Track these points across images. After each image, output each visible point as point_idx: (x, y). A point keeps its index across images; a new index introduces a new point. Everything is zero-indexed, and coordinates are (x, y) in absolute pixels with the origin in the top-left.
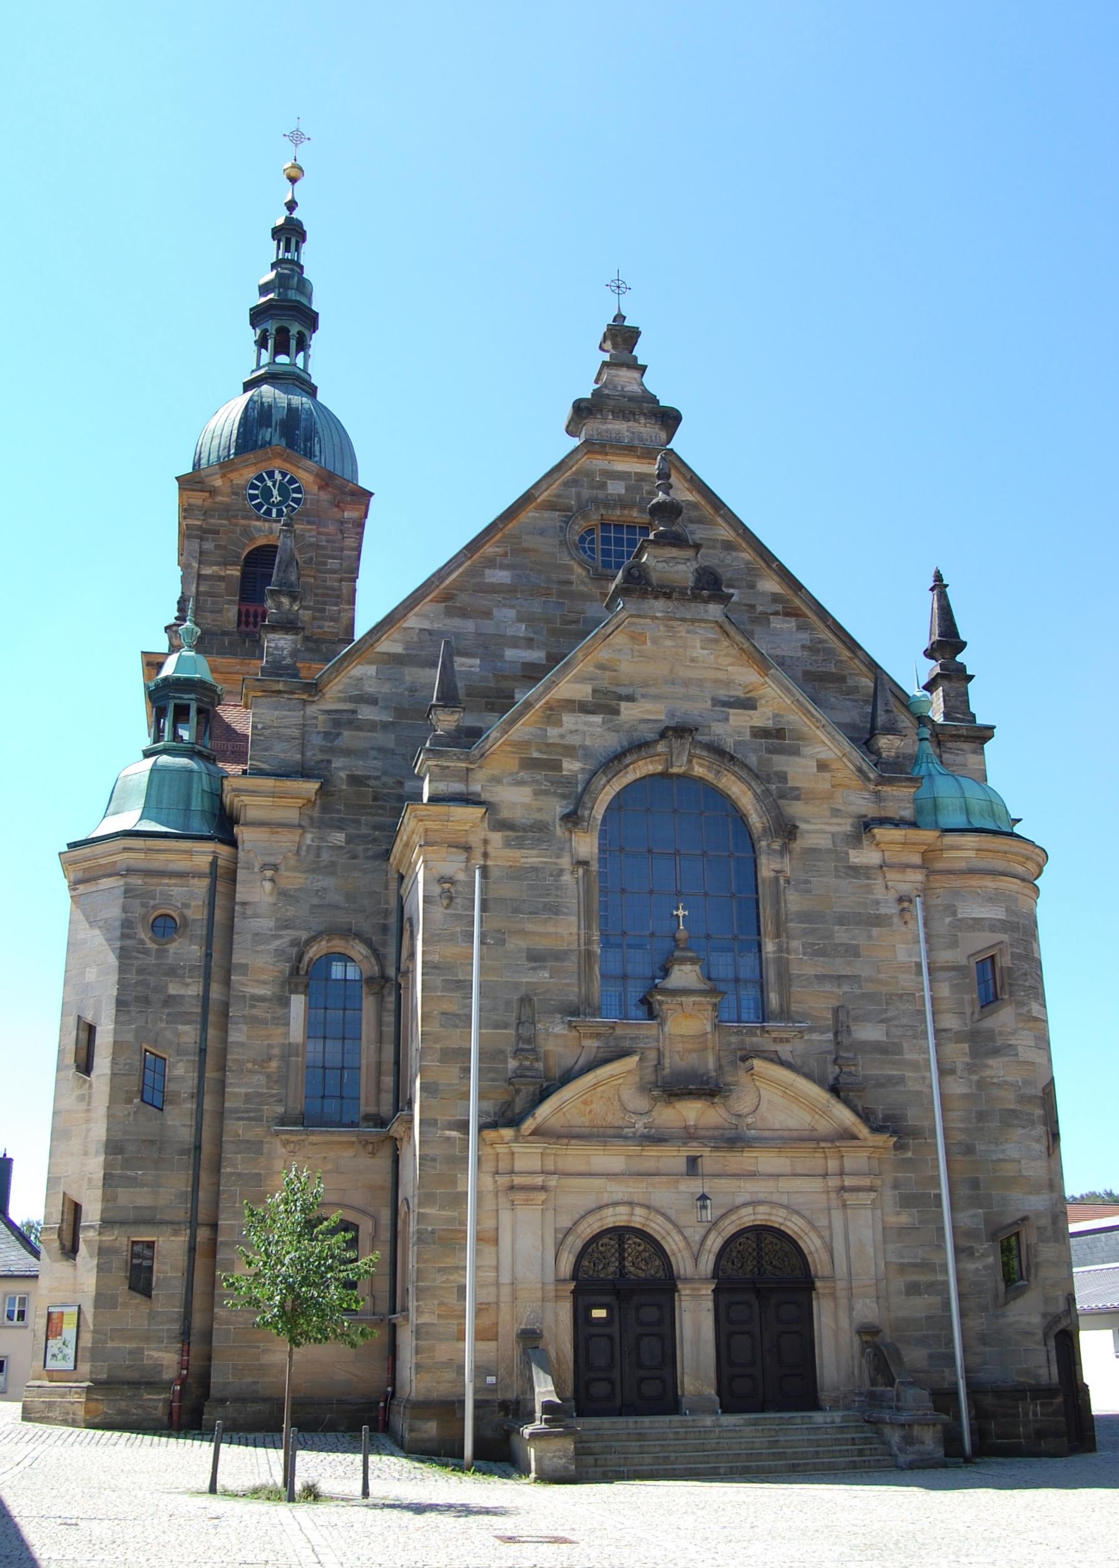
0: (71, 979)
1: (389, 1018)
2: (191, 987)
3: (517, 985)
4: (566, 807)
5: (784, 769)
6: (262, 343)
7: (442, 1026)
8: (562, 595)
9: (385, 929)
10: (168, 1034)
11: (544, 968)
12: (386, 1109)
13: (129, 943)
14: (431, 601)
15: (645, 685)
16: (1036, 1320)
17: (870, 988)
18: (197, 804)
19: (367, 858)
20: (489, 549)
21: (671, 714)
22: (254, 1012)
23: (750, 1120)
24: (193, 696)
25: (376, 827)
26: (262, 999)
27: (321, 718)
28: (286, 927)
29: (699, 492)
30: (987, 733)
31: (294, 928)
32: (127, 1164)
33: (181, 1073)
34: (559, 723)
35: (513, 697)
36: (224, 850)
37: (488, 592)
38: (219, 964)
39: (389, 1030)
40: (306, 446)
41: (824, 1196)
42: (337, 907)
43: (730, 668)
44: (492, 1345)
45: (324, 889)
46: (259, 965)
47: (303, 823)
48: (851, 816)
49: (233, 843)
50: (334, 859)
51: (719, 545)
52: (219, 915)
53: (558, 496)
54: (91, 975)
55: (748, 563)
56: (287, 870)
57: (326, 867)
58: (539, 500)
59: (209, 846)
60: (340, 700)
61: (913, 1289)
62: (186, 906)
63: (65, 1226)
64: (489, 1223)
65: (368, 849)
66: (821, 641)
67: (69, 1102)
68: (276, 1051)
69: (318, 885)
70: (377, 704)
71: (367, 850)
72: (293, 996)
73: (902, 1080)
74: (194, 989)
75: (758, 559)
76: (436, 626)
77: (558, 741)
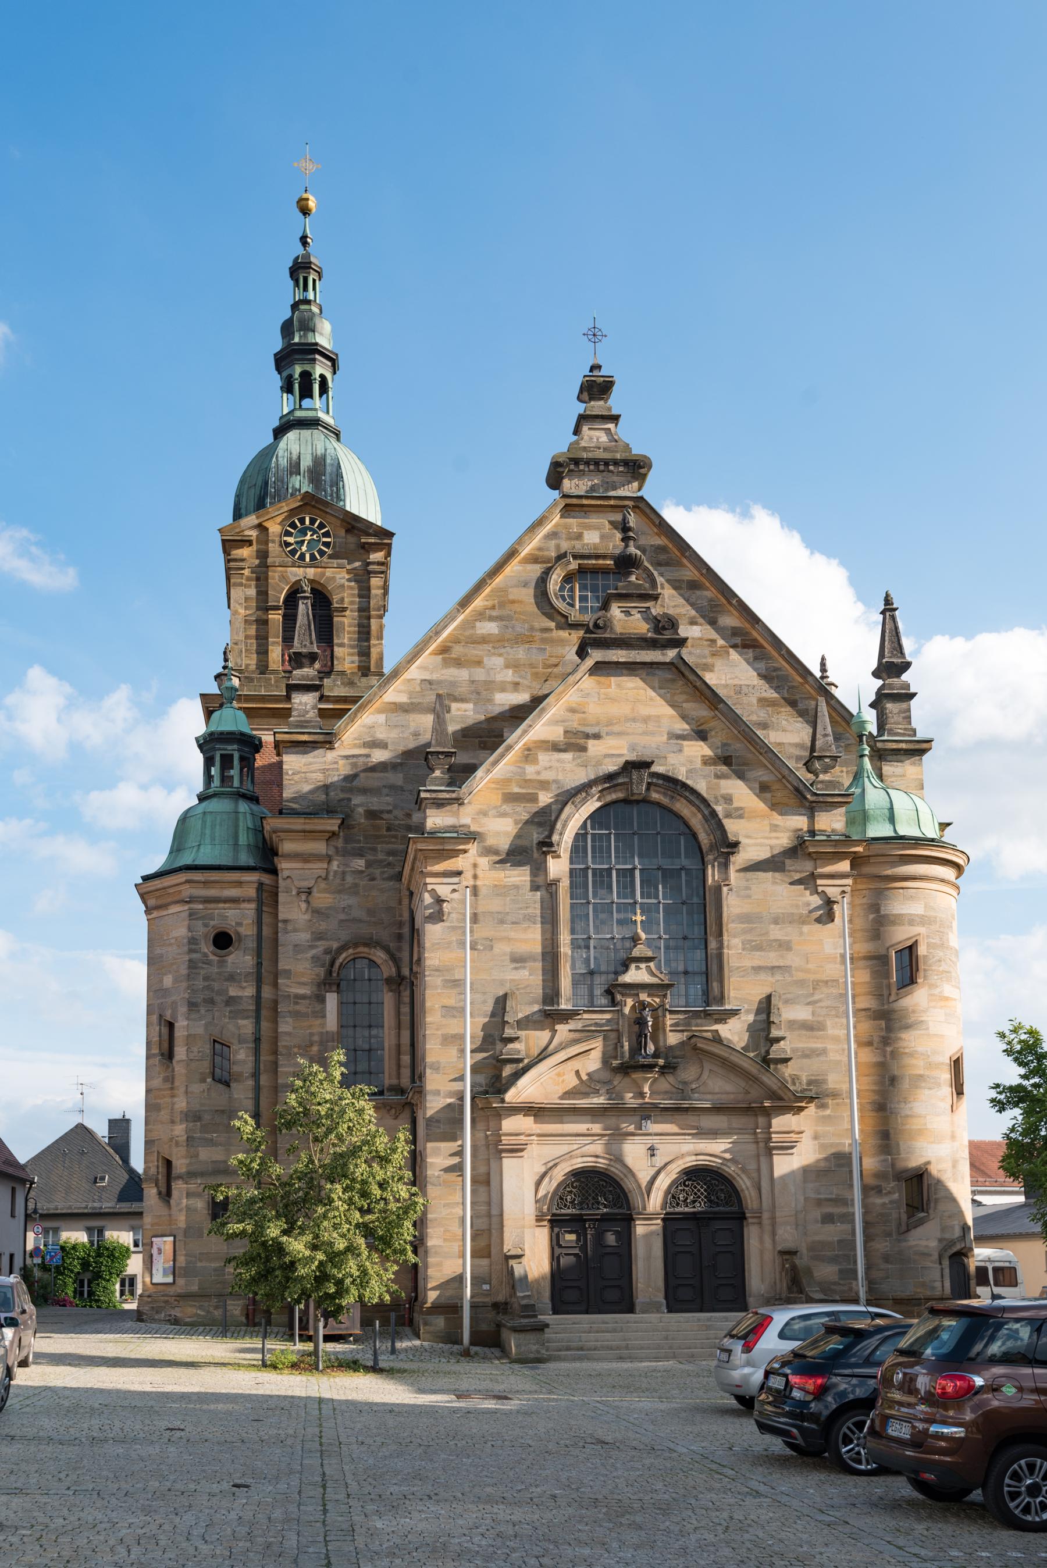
0: (155, 989)
1: (405, 1009)
2: (247, 990)
3: (502, 983)
4: (542, 833)
5: (730, 791)
6: (288, 388)
7: (443, 1016)
8: (544, 641)
9: (400, 937)
10: (231, 1027)
11: (524, 968)
12: (405, 1081)
13: (194, 956)
14: (430, 654)
15: (610, 723)
16: (933, 1244)
17: (800, 976)
18: (243, 839)
19: (384, 879)
20: (478, 603)
22: (297, 1007)
23: (694, 1086)
24: (235, 747)
25: (391, 853)
26: (303, 997)
27: (341, 762)
28: (320, 939)
29: (667, 537)
30: (925, 746)
31: (327, 939)
32: (205, 1129)
33: (242, 1056)
34: (535, 761)
35: (502, 736)
36: (266, 879)
37: (479, 643)
38: (266, 970)
39: (406, 1019)
40: (332, 491)
41: (754, 1146)
42: (360, 921)
43: (684, 705)
44: (485, 1262)
45: (350, 906)
46: (299, 971)
47: (330, 853)
48: (789, 830)
49: (274, 871)
50: (357, 881)
51: (684, 586)
52: (266, 931)
53: (540, 549)
54: (168, 981)
55: (711, 600)
56: (319, 892)
57: (350, 888)
58: (522, 555)
59: (253, 877)
60: (355, 746)
61: (828, 1219)
62: (239, 924)
63: (160, 1177)
64: (482, 1169)
65: (383, 872)
66: (776, 669)
67: (157, 1082)
68: (316, 1038)
69: (343, 904)
70: (387, 748)
71: (383, 872)
72: (328, 994)
73: (824, 1052)
74: (250, 991)
75: (719, 596)
76: (435, 677)
77: (534, 777)
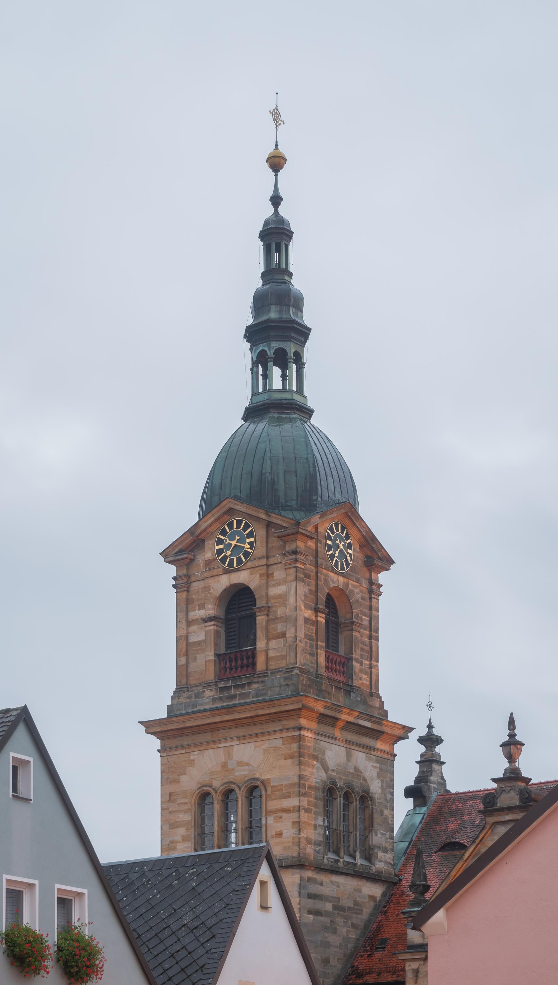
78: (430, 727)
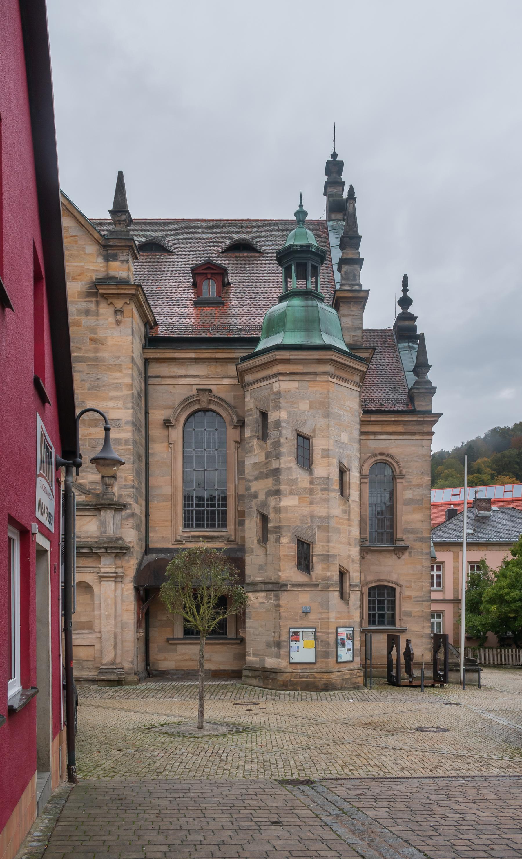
21: (175, 650)
30: (432, 391)
78: (334, 155)
